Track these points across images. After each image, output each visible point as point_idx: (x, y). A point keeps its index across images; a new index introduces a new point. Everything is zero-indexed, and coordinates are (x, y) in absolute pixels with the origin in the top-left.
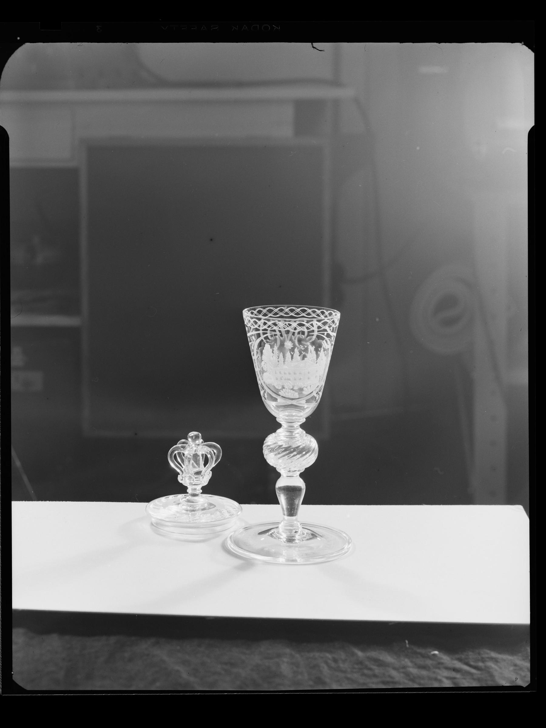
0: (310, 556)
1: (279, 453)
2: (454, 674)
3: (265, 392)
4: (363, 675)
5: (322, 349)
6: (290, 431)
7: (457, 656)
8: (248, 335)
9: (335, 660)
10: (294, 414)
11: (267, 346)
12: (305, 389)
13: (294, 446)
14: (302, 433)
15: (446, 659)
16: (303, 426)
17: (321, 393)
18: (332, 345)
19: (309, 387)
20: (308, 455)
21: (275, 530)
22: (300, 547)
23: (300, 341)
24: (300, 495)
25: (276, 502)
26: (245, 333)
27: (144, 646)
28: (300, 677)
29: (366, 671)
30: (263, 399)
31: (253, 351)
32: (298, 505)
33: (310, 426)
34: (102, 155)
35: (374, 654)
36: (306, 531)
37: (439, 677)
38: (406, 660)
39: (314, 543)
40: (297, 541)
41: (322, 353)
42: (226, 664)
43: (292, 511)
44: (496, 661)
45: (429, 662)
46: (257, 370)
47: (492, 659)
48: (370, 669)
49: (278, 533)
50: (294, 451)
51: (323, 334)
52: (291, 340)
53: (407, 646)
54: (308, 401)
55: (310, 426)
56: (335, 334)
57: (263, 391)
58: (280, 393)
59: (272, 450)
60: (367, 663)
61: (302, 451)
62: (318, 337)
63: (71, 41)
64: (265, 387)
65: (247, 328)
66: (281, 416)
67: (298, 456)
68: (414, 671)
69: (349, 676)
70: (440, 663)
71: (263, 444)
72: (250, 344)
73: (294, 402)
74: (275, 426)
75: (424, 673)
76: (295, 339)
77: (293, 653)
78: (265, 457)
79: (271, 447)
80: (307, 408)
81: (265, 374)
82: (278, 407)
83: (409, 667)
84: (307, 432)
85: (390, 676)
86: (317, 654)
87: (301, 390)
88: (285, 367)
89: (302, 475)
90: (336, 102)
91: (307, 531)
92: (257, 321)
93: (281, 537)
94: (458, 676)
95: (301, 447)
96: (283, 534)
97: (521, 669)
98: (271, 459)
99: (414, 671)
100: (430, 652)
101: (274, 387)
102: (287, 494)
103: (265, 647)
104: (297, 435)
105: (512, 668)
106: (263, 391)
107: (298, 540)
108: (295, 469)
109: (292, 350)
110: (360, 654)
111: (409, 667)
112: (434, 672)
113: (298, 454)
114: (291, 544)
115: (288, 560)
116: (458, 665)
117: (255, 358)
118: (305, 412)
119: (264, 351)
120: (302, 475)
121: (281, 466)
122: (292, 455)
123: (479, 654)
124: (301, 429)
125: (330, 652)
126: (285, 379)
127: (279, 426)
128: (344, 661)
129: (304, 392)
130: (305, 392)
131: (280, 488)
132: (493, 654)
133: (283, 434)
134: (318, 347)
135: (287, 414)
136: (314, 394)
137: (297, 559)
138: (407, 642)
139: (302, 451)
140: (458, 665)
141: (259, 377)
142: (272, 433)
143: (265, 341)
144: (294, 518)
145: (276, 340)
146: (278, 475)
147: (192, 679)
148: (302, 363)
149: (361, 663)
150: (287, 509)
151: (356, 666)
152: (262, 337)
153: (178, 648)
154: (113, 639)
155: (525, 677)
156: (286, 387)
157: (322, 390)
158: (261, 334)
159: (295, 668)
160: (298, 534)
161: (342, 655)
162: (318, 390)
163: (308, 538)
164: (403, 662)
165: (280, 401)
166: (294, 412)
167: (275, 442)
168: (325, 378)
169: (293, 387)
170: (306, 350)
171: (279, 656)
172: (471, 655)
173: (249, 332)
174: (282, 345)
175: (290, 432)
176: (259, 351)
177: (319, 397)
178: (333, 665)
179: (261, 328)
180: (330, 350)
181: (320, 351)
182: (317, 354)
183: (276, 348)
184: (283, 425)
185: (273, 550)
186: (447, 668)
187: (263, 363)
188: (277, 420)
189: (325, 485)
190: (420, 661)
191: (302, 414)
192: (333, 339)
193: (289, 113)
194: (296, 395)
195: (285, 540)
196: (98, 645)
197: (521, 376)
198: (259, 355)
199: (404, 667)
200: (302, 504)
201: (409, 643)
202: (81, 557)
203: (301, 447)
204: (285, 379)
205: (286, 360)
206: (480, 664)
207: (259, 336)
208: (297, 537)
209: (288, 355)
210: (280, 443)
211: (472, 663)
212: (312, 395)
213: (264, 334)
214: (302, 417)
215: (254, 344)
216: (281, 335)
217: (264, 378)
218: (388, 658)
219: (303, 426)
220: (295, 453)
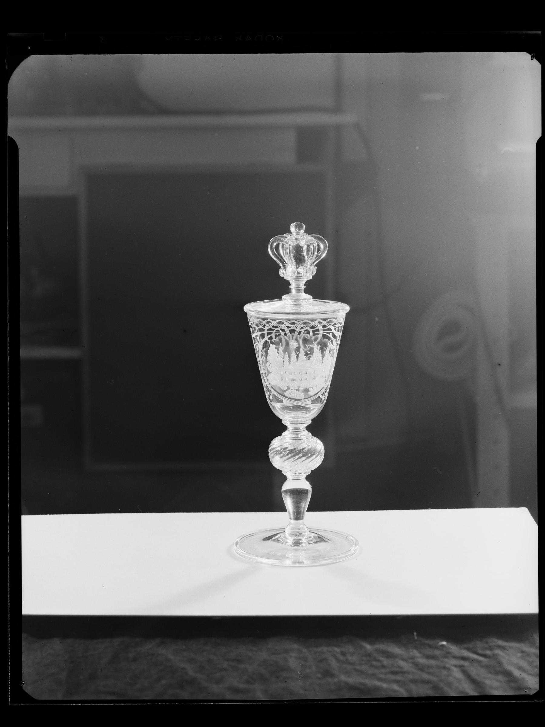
0: (316, 558)
1: (284, 456)
2: (462, 662)
3: (270, 394)
4: (372, 666)
5: (328, 349)
6: (296, 432)
7: (465, 646)
8: (253, 336)
9: (343, 654)
10: (300, 416)
11: (272, 347)
12: (310, 389)
13: (299, 448)
14: (308, 434)
15: (454, 649)
16: (309, 428)
17: (327, 394)
18: (337, 345)
19: (314, 387)
20: (314, 457)
21: (281, 534)
22: (305, 550)
23: (305, 341)
24: (307, 497)
25: (283, 509)
26: (250, 334)
27: (149, 646)
28: (308, 671)
29: (374, 663)
30: (269, 401)
31: (258, 352)
32: (303, 513)
33: (316, 428)
34: (98, 181)
35: (382, 646)
36: (312, 535)
37: (448, 666)
38: (415, 651)
39: (321, 546)
40: (304, 545)
41: (327, 353)
42: (233, 660)
43: (298, 516)
44: (503, 648)
45: (437, 652)
46: (262, 371)
47: (499, 647)
48: (379, 661)
49: (284, 537)
50: (298, 454)
51: (329, 333)
52: (296, 339)
53: (416, 638)
54: (313, 402)
55: (316, 428)
56: (340, 334)
57: (268, 393)
58: (286, 394)
59: (277, 453)
60: (376, 655)
61: (308, 453)
62: (324, 336)
63: (67, 54)
64: (271, 389)
65: (251, 329)
66: (286, 418)
67: (304, 458)
68: (422, 661)
69: (358, 667)
70: (448, 653)
71: (269, 447)
72: (255, 345)
73: (300, 403)
74: (279, 428)
75: (432, 662)
76: (300, 338)
77: (301, 648)
78: (271, 460)
79: (276, 449)
80: (314, 409)
81: (270, 375)
82: (284, 408)
83: (418, 657)
84: (313, 435)
85: (398, 667)
86: (325, 649)
87: (306, 391)
88: (291, 367)
89: (308, 478)
90: (338, 129)
91: (313, 534)
92: (262, 321)
93: (288, 541)
94: (466, 664)
95: (306, 449)
96: (289, 538)
97: (528, 655)
98: (277, 462)
99: (422, 661)
100: (438, 643)
101: (280, 388)
102: (293, 498)
103: (273, 644)
104: (302, 437)
105: (519, 655)
106: (268, 393)
107: (305, 543)
108: (300, 472)
109: (298, 349)
110: (368, 647)
111: (418, 657)
112: (442, 661)
113: (303, 456)
114: (297, 548)
115: (294, 562)
116: (466, 654)
117: (260, 359)
118: (311, 414)
119: (269, 351)
120: (308, 478)
121: (286, 469)
122: (297, 457)
123: (487, 643)
124: (306, 431)
125: (339, 646)
126: (291, 380)
127: (285, 428)
128: (353, 654)
129: (309, 393)
130: (311, 393)
131: (286, 492)
132: (500, 643)
133: (289, 436)
134: (323, 347)
135: (293, 415)
136: (320, 395)
137: (303, 560)
138: (415, 634)
139: (308, 453)
140: (466, 654)
141: (264, 378)
142: (277, 436)
143: (269, 341)
144: (300, 521)
145: (281, 340)
146: (284, 478)
147: (198, 675)
148: (308, 363)
149: (369, 655)
150: (294, 513)
151: (364, 658)
152: (266, 338)
153: (184, 647)
154: (117, 641)
155: (532, 662)
156: (291, 388)
157: (328, 391)
158: (266, 335)
159: (303, 663)
160: (305, 537)
161: (350, 648)
162: (324, 390)
163: (315, 541)
164: (411, 653)
165: (286, 402)
166: (300, 414)
167: (280, 444)
168: (330, 379)
169: (299, 387)
170: (312, 350)
171: (286, 651)
172: (479, 645)
173: (253, 333)
174: (287, 344)
175: (296, 434)
176: (264, 353)
177: (324, 398)
178: (341, 658)
179: (266, 328)
180: (335, 351)
181: (325, 351)
182: (322, 353)
183: (281, 348)
184: (288, 427)
185: (280, 554)
186: (455, 657)
187: (268, 364)
188: (283, 422)
189: (332, 492)
190: (429, 652)
191: (307, 415)
192: (339, 339)
193: (290, 139)
194: (302, 396)
195: (291, 544)
196: (103, 648)
197: (528, 399)
198: (264, 357)
199: (413, 658)
200: (308, 511)
201: (417, 635)
202: (84, 564)
203: (306, 449)
204: (291, 380)
205: (292, 360)
206: (488, 652)
207: (263, 336)
208: (304, 540)
209: (294, 355)
210: (285, 446)
211: (480, 652)
212: (317, 396)
213: (268, 334)
214: (308, 418)
215: (259, 346)
216: (286, 335)
217: (269, 379)
218: (396, 650)
219: (309, 428)
220: (301, 455)
